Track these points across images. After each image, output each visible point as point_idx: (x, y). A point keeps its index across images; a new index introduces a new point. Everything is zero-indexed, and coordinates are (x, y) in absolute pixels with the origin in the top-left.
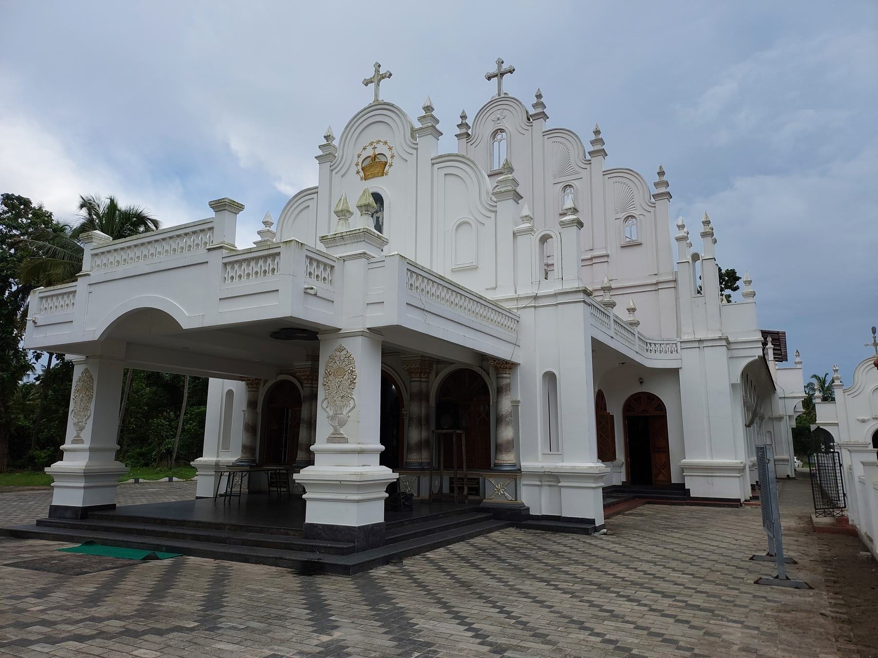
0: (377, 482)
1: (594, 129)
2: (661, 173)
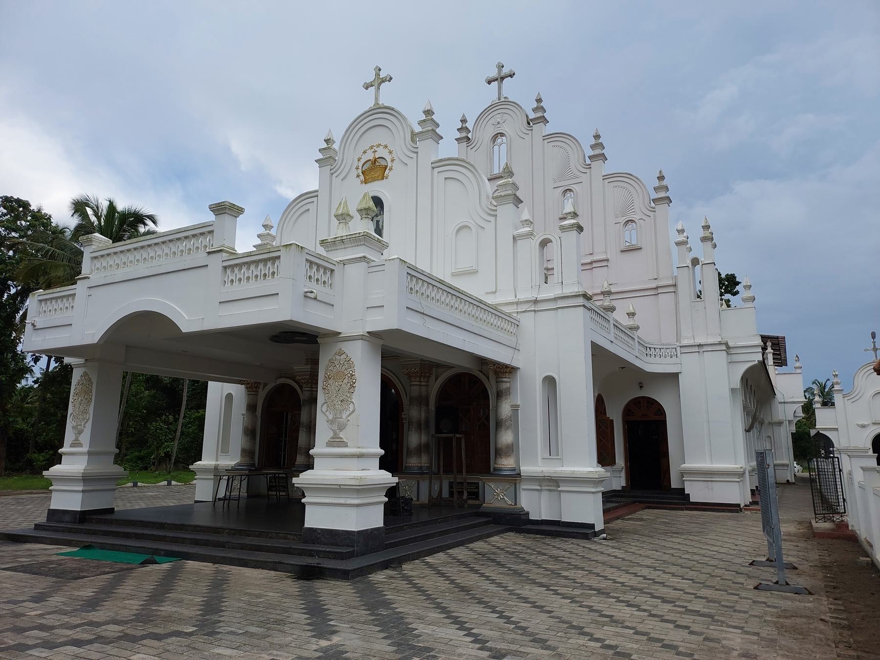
0: (93, 477)
1: (593, 133)
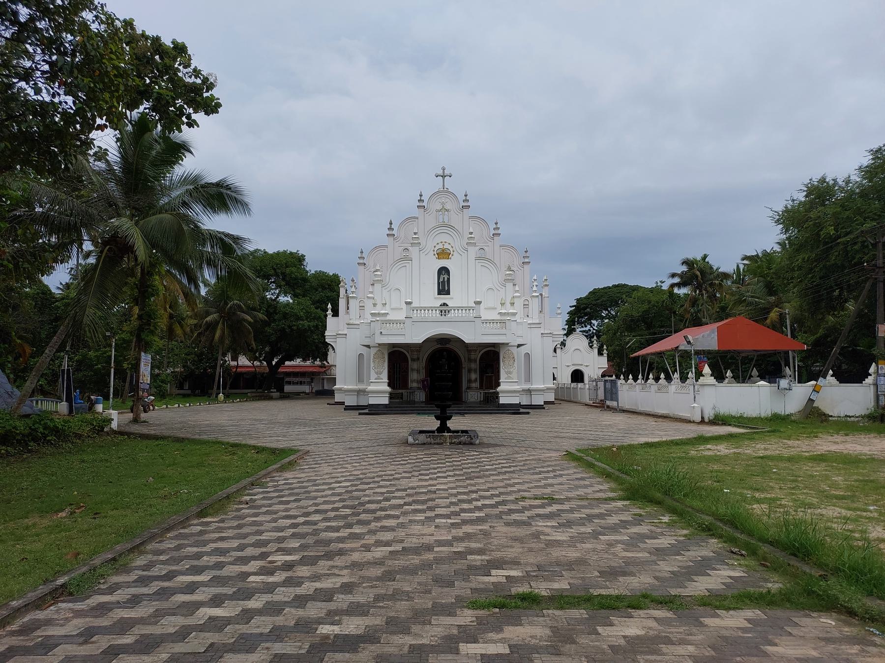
2: (466, 196)
